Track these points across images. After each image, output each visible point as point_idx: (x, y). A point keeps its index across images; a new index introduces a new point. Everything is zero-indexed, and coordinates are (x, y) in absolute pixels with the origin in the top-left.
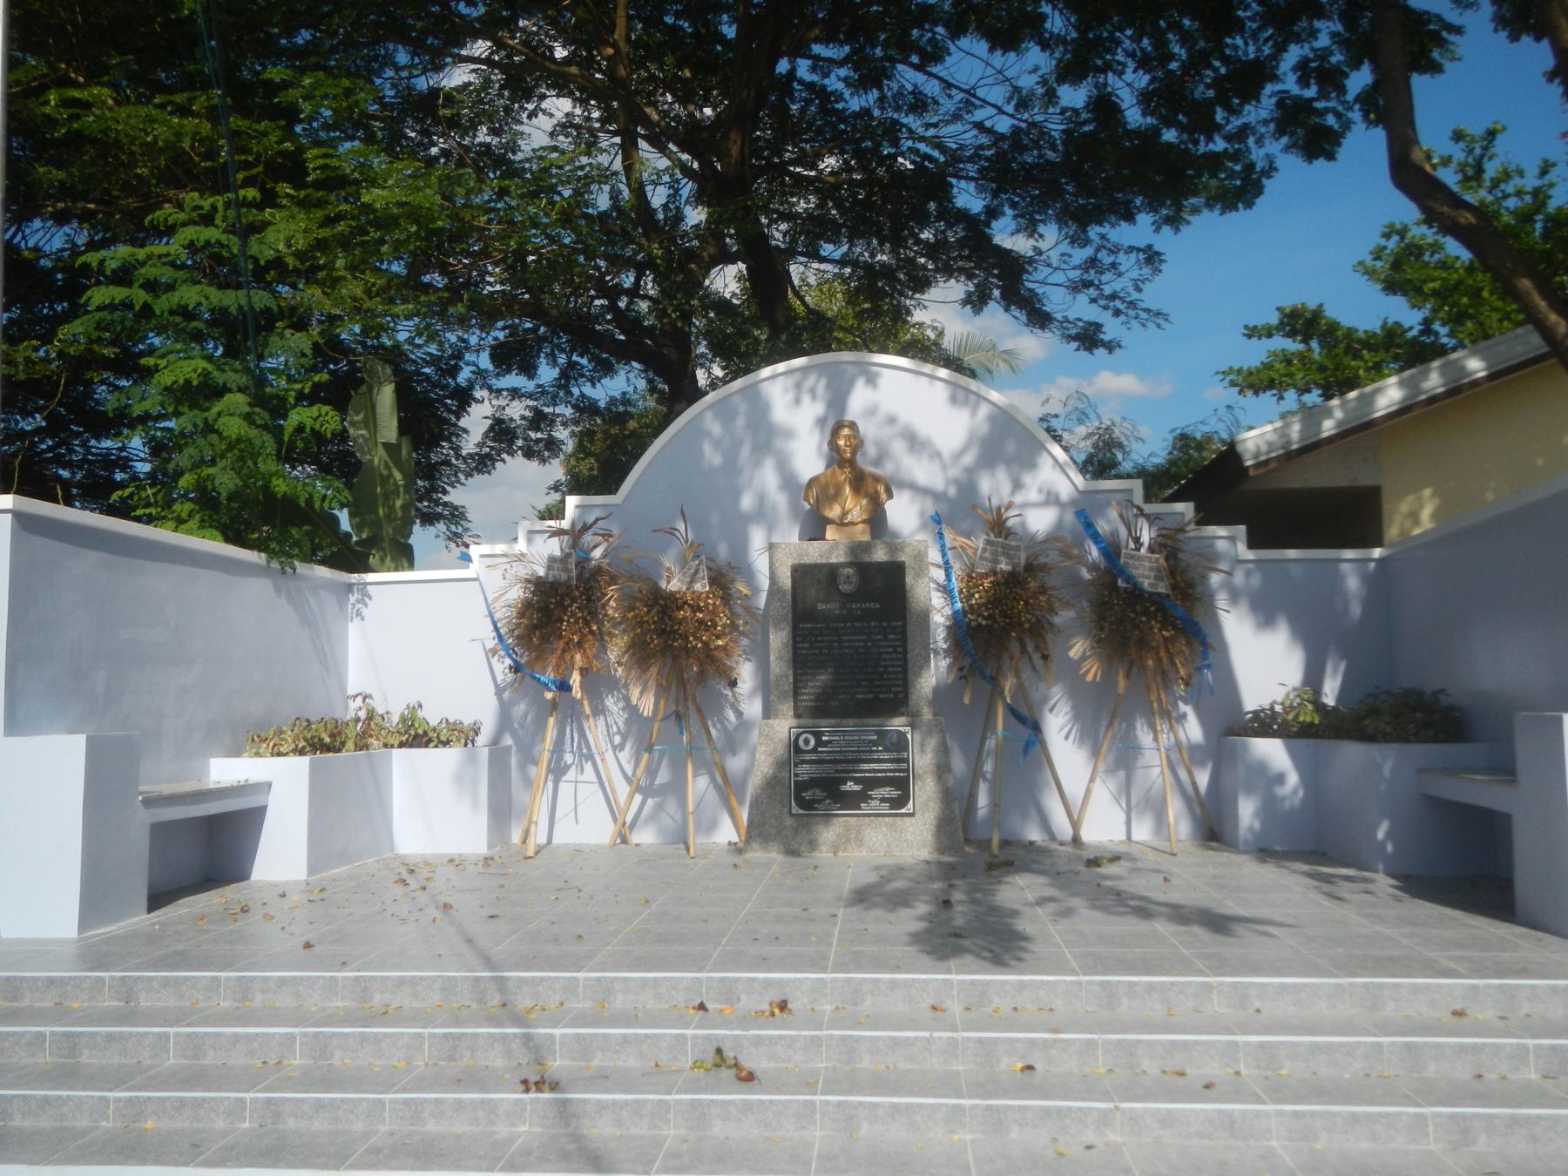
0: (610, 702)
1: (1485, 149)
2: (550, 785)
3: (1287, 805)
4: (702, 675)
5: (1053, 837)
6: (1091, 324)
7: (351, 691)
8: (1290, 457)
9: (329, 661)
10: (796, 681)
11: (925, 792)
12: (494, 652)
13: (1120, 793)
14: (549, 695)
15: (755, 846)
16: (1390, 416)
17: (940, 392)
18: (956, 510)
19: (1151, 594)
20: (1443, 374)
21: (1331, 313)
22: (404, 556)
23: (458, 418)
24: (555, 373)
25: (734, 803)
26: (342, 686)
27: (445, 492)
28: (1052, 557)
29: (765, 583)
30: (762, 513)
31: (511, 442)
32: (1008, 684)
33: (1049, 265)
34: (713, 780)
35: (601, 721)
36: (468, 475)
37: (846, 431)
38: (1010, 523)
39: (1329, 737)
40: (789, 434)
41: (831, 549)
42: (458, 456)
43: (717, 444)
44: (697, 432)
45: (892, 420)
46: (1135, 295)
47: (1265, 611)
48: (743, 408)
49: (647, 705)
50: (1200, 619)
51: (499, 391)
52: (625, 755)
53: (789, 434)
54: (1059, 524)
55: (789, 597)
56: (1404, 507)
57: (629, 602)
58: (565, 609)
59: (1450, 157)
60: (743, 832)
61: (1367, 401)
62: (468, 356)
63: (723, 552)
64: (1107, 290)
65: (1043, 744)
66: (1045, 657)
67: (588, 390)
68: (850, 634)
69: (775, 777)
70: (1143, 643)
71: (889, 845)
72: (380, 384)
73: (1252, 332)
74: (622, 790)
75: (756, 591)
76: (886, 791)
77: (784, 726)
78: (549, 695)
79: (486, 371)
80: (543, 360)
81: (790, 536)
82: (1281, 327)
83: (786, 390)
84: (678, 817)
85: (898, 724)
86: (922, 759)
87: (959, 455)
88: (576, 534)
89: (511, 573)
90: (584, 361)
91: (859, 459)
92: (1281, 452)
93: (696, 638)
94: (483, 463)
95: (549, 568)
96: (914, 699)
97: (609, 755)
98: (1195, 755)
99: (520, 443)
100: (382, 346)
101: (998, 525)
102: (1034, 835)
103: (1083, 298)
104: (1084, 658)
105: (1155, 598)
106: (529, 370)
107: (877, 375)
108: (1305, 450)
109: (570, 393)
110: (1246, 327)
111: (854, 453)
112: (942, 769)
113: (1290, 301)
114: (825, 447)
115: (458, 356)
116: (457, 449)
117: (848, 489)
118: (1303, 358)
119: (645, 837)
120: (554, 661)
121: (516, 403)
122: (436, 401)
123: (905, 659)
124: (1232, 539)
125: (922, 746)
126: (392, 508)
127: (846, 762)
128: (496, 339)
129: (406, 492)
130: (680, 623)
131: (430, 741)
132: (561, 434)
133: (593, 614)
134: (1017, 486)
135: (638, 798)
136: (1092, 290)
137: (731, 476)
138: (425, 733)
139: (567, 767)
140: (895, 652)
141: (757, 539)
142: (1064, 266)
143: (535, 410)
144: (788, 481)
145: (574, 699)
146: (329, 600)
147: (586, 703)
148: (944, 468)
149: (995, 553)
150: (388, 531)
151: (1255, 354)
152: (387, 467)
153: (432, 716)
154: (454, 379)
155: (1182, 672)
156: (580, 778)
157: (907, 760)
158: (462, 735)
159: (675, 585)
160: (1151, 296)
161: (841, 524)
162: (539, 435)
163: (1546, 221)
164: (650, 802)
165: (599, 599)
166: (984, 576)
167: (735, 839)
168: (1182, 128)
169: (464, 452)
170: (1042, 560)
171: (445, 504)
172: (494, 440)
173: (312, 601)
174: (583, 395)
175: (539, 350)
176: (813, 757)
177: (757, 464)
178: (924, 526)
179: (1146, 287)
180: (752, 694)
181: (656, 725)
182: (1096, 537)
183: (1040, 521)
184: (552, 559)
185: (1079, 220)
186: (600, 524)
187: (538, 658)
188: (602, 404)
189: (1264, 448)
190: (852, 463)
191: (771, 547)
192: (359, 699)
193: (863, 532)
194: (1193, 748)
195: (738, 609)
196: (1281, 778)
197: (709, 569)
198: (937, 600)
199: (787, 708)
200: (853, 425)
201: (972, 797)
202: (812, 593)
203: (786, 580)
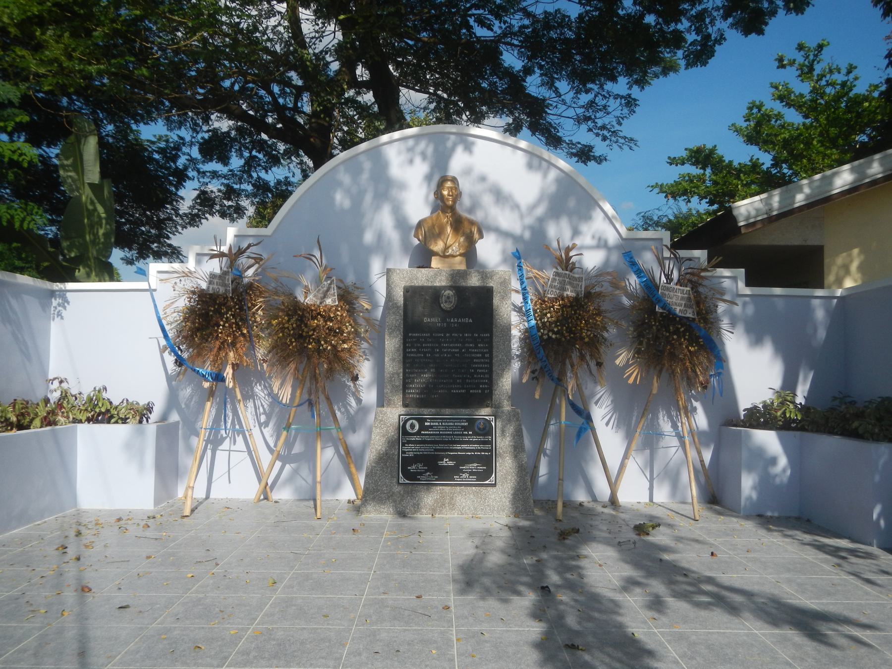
0: (258, 389)
1: (816, 56)
2: (209, 452)
3: (778, 481)
4: (331, 370)
5: (595, 500)
6: (586, 146)
7: (51, 377)
8: (771, 220)
9: (31, 351)
10: (405, 378)
11: (505, 466)
12: (165, 348)
13: (646, 467)
14: (206, 385)
15: (370, 508)
16: (842, 193)
17: (520, 158)
18: (528, 249)
19: (681, 318)
20: (882, 165)
21: (720, 152)
22: (107, 272)
23: (177, 190)
24: (242, 162)
25: (353, 470)
26: (44, 371)
27: (168, 238)
28: (606, 288)
29: (382, 300)
30: (380, 246)
31: (212, 206)
32: (571, 385)
33: (565, 104)
34: (337, 451)
35: (250, 404)
36: (184, 227)
37: (449, 184)
38: (573, 259)
39: (812, 431)
40: (402, 186)
41: (436, 275)
42: (177, 215)
43: (348, 191)
44: (332, 183)
45: (483, 179)
46: (617, 127)
47: (756, 333)
48: (367, 165)
49: (286, 395)
50: (714, 337)
51: (204, 173)
52: (268, 431)
53: (402, 186)
54: (607, 262)
55: (401, 312)
56: (840, 260)
57: (272, 312)
58: (222, 315)
59: (794, 60)
60: (360, 493)
61: (828, 181)
62: (184, 149)
63: (350, 279)
64: (600, 123)
65: (593, 430)
66: (599, 364)
67: (263, 174)
68: (448, 341)
69: (386, 453)
70: (673, 357)
71: (476, 509)
72: (86, 137)
73: (673, 161)
74: (265, 458)
75: (375, 305)
76: (473, 466)
77: (395, 413)
78: (206, 385)
79: (196, 159)
80: (234, 154)
81: (402, 264)
82: (689, 159)
83: (399, 153)
84: (310, 479)
85: (484, 413)
86: (503, 442)
87: (533, 207)
88: (234, 255)
89: (180, 285)
90: (261, 156)
91: (457, 207)
92: (765, 216)
93: (326, 342)
94: (193, 220)
95: (210, 283)
96: (497, 393)
97: (256, 431)
98: (700, 439)
99: (218, 207)
100: (170, 167)
101: (566, 263)
102: (581, 496)
103: (584, 127)
104: (627, 366)
105: (684, 321)
106: (224, 160)
107: (473, 143)
108: (782, 215)
109: (251, 177)
110: (669, 158)
111: (454, 202)
112: (518, 448)
113: (693, 145)
114: (432, 197)
115: (177, 148)
116: (176, 210)
117: (449, 229)
118: (702, 179)
119: (284, 495)
120: (212, 358)
121: (214, 181)
122: (162, 177)
123: (491, 363)
124: (734, 278)
125: (503, 431)
126: (96, 235)
127: (445, 442)
128: (203, 138)
129: (107, 223)
130: (314, 330)
131: (112, 417)
132: (245, 203)
133: (244, 321)
134: (576, 232)
135: (278, 464)
136: (589, 123)
137: (356, 218)
138: (108, 411)
139: (223, 440)
140: (483, 357)
141: (376, 266)
142: (574, 105)
143: (227, 186)
144: (401, 223)
145: (227, 388)
146: (33, 304)
147: (237, 390)
148: (522, 217)
149: (563, 283)
150: (93, 252)
151: (672, 175)
152: (92, 203)
153: (115, 396)
154: (175, 163)
155: (701, 378)
156: (233, 448)
157: (491, 443)
158: (142, 413)
159: (310, 300)
160: (627, 129)
161: (444, 256)
162: (230, 203)
163: (847, 102)
164: (288, 467)
165: (250, 309)
166: (553, 300)
167: (353, 497)
168: (658, 14)
169: (181, 212)
170: (597, 289)
171: (170, 246)
172: (200, 205)
173: (13, 302)
174: (259, 178)
175: (232, 147)
176: (418, 438)
177: (377, 208)
178: (505, 261)
179: (625, 122)
180: (369, 386)
181: (294, 409)
182: (639, 272)
183: (592, 260)
184: (213, 276)
185: (582, 79)
186: (252, 249)
187: (199, 354)
188: (272, 184)
189: (753, 213)
190: (452, 209)
191: (388, 272)
192: (56, 383)
193: (461, 263)
194: (701, 434)
195: (361, 321)
196: (773, 461)
197: (339, 288)
198: (515, 318)
199: (398, 399)
200: (454, 180)
201: (536, 468)
202: (420, 309)
203: (399, 295)
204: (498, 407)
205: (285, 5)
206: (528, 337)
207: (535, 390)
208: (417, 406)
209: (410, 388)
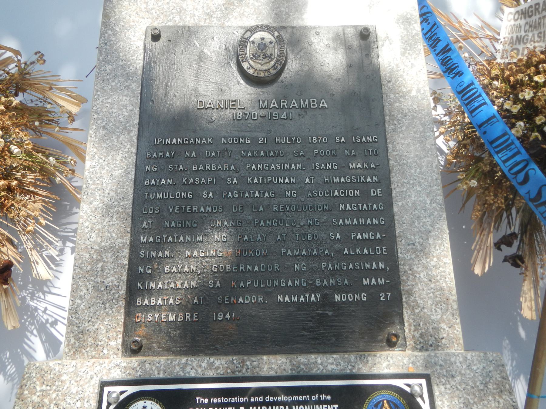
199: (110, 330)
204: (429, 342)
205: (10, 328)
206: (474, 152)
207: (517, 293)
208: (169, 351)
209: (150, 292)
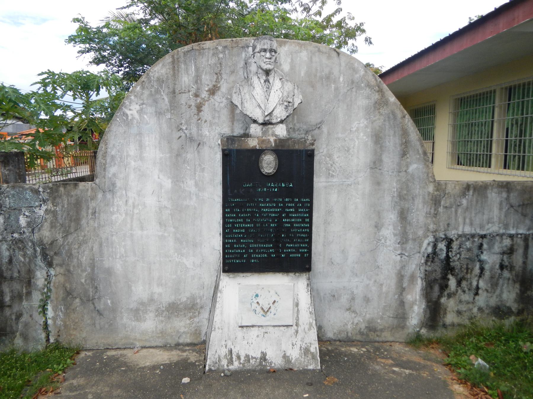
140: (303, 222)
